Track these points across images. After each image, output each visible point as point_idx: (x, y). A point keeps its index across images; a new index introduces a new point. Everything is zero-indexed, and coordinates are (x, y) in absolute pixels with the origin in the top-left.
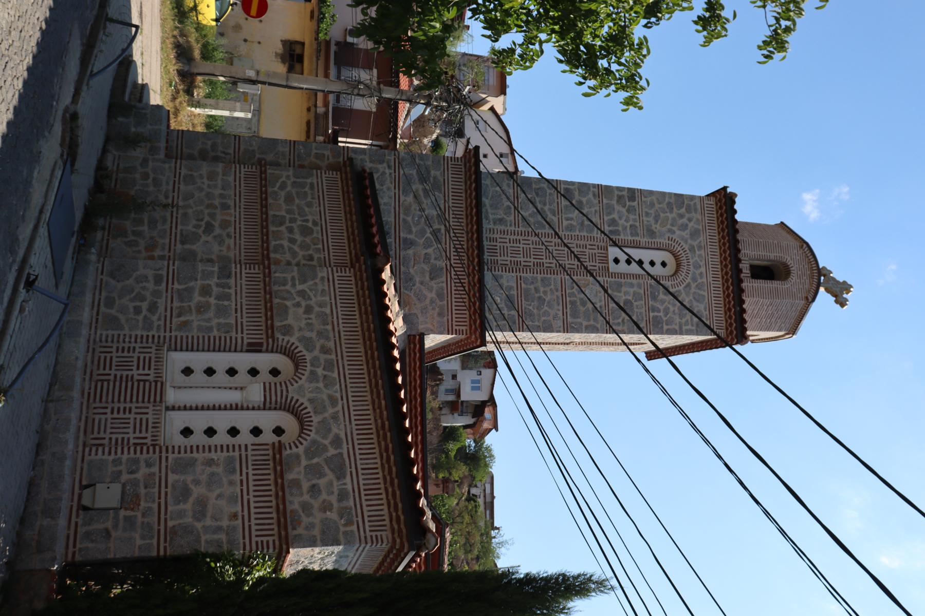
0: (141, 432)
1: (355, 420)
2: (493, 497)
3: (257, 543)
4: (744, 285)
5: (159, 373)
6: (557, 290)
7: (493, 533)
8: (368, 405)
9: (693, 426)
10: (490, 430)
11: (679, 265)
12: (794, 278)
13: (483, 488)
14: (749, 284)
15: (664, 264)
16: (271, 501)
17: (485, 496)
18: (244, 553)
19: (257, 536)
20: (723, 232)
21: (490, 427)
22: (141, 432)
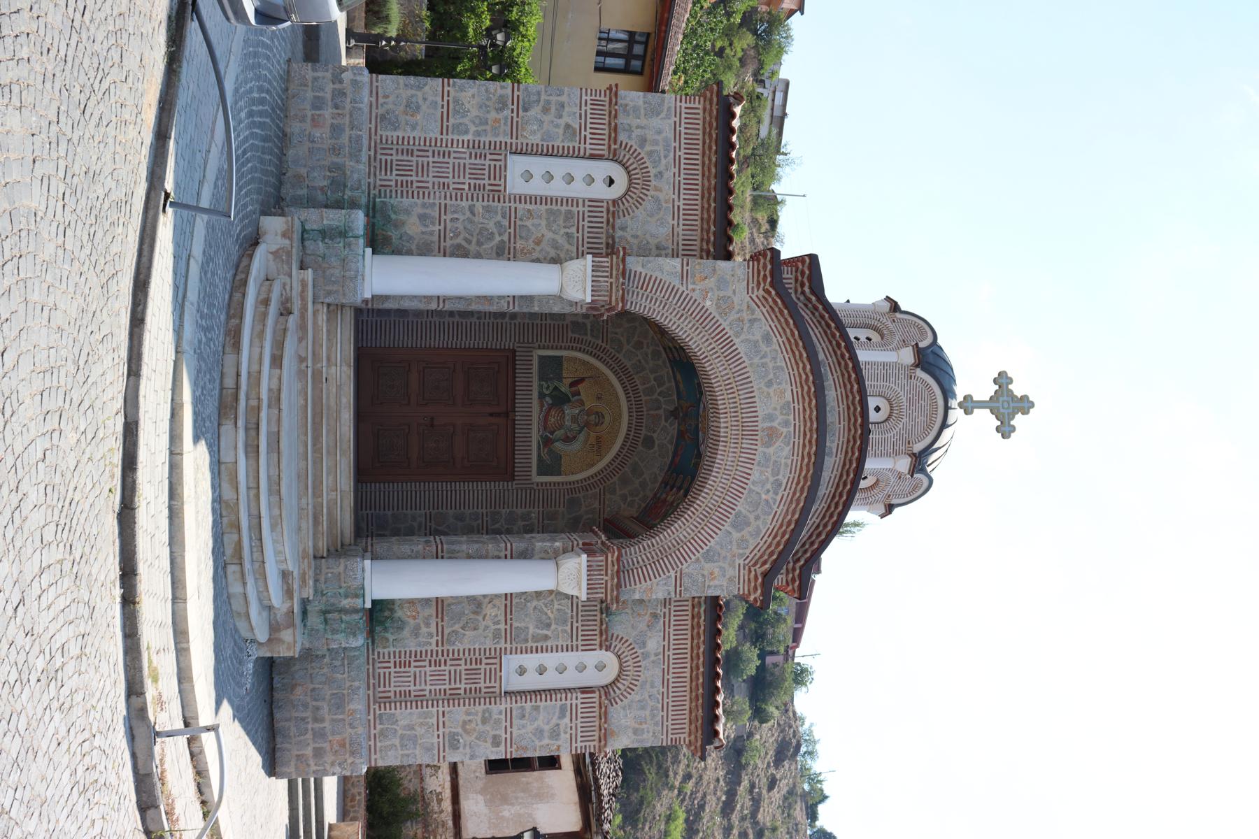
0: (490, 669)
1: (591, 128)
2: (784, 115)
3: (672, 739)
7: (780, 157)
10: (796, 11)
13: (772, 89)
16: (596, 615)
17: (772, 109)
18: (372, 540)
19: (672, 734)
20: (793, 584)
21: (795, 8)
22: (490, 669)
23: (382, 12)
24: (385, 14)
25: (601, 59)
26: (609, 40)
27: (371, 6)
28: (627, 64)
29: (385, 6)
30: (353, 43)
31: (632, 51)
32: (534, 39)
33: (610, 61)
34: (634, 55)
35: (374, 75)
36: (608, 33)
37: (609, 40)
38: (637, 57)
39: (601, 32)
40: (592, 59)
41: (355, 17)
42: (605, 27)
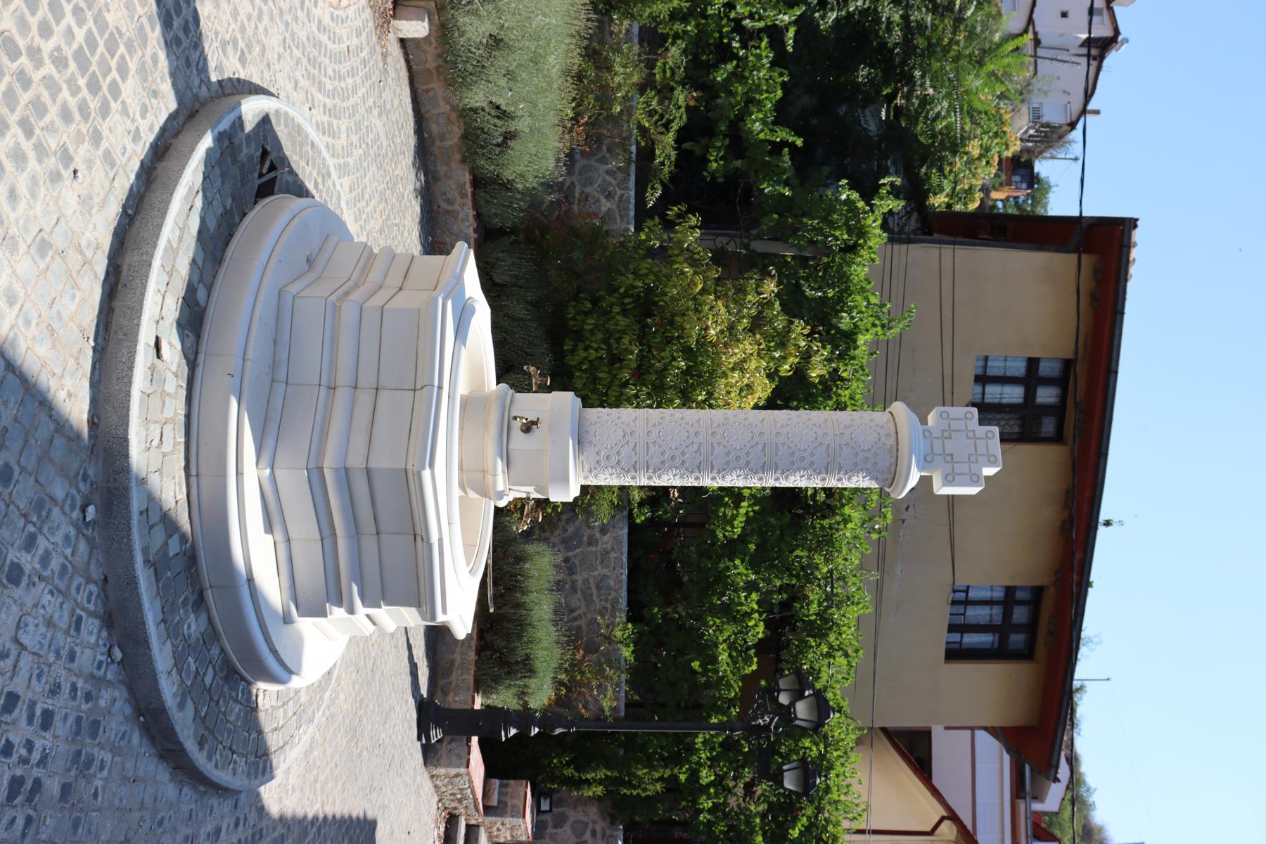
23: (513, 650)
24: (519, 655)
25: (956, 637)
26: (967, 602)
27: (489, 637)
28: (1003, 640)
29: (520, 637)
30: (436, 735)
31: (203, 68)
32: (856, 651)
33: (971, 639)
34: (1004, 619)
35: (496, 783)
36: (967, 592)
37: (967, 602)
38: (1018, 628)
39: (954, 591)
40: (941, 638)
41: (453, 661)
42: (961, 582)
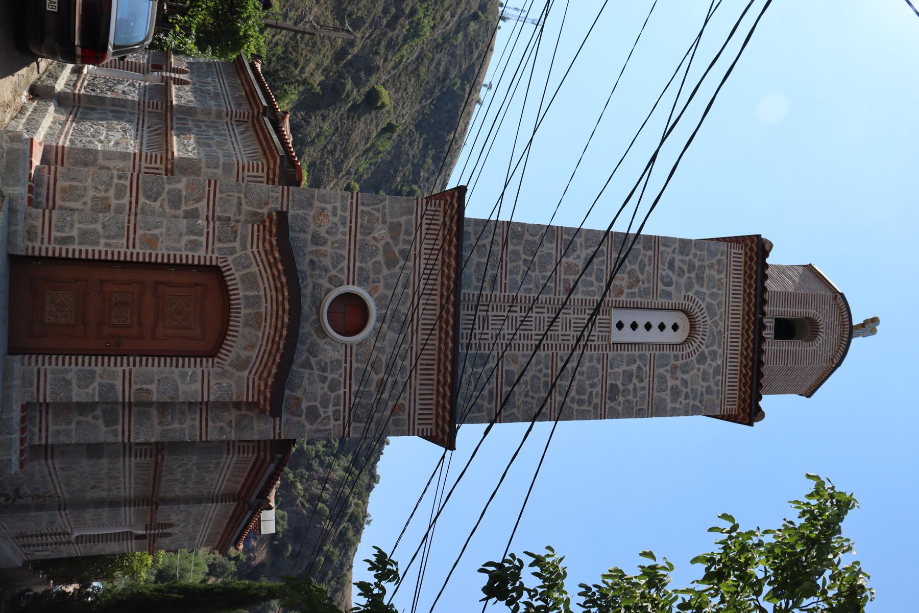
4: (765, 347)
5: (111, 538)
6: (547, 368)
8: (741, 266)
9: (403, 532)
11: (693, 327)
12: (822, 337)
14: (773, 347)
15: (675, 327)
19: (419, 424)
